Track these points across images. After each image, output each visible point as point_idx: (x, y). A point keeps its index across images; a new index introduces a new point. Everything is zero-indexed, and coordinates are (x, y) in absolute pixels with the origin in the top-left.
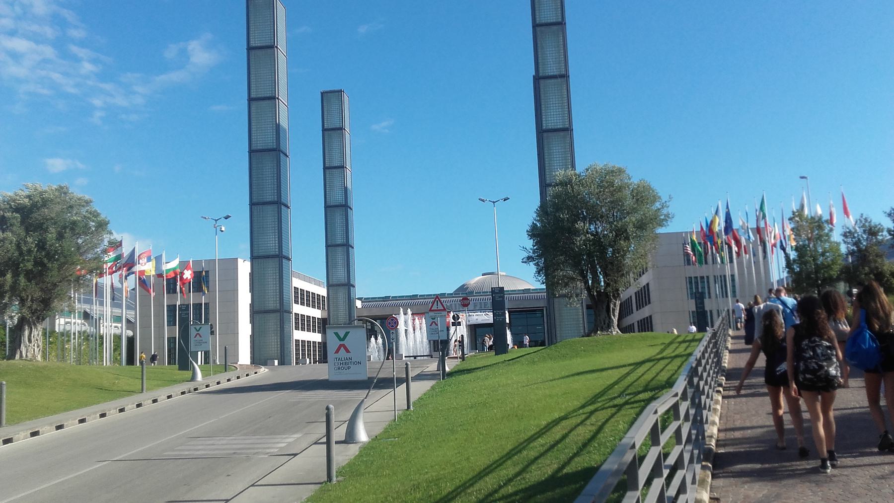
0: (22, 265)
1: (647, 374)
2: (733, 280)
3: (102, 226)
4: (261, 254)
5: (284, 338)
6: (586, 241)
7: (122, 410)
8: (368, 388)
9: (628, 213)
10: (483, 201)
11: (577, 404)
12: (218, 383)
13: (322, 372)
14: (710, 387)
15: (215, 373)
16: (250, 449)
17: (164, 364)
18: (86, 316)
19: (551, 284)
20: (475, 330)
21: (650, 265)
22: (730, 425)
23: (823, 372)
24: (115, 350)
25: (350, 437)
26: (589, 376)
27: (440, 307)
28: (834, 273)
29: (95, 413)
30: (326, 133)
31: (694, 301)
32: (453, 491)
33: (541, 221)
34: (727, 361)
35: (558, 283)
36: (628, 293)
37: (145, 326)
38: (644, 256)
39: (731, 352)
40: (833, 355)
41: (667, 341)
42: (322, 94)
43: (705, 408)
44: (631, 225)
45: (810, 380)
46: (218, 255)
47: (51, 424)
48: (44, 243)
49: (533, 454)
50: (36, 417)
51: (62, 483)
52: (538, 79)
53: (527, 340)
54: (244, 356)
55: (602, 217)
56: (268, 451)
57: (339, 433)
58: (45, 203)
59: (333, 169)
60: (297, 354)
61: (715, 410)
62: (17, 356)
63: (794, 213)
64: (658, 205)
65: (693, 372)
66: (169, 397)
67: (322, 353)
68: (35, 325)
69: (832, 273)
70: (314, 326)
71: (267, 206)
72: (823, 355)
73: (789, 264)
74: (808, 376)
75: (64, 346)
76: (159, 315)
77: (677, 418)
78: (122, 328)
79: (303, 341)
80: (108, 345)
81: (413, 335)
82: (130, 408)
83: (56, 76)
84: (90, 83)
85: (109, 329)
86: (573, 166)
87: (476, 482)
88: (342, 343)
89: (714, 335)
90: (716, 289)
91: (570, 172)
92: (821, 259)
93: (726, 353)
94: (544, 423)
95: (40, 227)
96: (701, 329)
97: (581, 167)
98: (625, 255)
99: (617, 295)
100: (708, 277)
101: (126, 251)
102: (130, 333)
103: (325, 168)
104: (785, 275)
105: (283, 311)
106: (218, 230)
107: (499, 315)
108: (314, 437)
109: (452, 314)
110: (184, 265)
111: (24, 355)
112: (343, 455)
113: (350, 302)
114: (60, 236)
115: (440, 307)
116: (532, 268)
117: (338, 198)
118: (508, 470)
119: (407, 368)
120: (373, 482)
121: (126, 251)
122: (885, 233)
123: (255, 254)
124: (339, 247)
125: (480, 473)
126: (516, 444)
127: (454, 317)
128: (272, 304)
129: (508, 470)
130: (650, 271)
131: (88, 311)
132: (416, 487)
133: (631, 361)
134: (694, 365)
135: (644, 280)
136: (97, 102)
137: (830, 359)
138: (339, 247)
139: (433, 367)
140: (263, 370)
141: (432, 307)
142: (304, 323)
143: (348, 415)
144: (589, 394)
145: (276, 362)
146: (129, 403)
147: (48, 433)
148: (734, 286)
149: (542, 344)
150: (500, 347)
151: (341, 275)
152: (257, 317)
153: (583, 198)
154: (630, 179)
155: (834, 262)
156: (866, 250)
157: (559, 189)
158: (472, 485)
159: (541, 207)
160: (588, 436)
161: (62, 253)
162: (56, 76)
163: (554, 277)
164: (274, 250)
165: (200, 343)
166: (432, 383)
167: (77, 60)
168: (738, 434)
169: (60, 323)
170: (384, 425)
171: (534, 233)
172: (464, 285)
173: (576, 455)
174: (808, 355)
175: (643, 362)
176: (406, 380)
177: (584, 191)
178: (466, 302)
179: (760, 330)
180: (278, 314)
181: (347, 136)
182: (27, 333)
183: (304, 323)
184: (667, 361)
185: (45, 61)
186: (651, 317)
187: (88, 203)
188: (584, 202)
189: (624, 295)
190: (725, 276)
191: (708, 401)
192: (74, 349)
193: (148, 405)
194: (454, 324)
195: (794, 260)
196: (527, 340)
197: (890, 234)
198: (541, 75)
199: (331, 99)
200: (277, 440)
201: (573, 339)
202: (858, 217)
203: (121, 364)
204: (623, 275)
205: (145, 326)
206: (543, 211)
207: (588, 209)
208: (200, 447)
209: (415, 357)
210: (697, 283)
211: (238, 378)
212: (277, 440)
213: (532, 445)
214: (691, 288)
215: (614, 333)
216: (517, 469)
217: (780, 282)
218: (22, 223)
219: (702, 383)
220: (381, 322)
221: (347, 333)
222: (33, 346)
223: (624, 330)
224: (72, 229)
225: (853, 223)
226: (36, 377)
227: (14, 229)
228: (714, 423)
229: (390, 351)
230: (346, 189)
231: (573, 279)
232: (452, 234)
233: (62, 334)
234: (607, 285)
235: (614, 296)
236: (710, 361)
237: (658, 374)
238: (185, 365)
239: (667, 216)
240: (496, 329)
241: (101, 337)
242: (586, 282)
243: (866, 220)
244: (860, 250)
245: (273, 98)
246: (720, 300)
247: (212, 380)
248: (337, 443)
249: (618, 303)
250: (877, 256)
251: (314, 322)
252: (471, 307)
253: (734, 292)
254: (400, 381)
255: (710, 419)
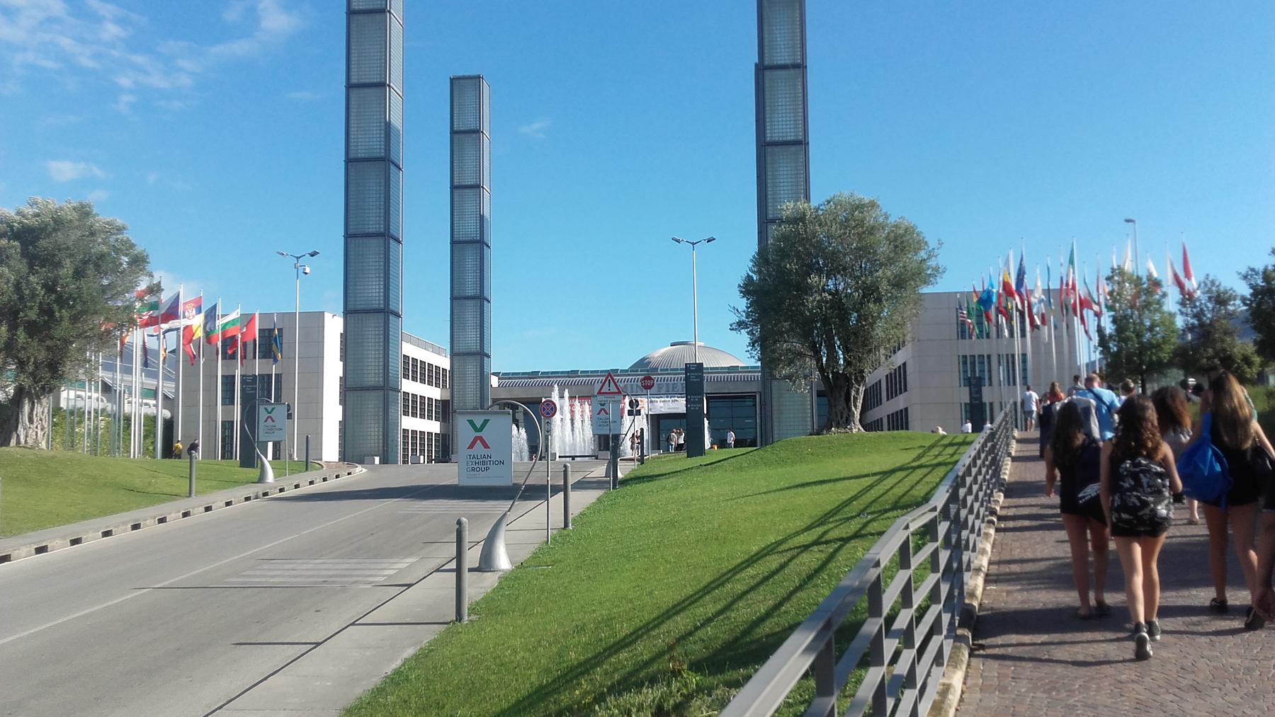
0: (21, 314)
1: (897, 487)
2: (1024, 361)
3: (139, 262)
4: (359, 307)
5: (388, 426)
6: (821, 302)
7: (162, 521)
8: (512, 498)
9: (881, 265)
10: (678, 241)
11: (800, 524)
12: (297, 486)
13: (447, 474)
14: (977, 517)
15: (292, 472)
16: (345, 576)
17: (215, 458)
18: (107, 389)
19: (769, 362)
20: (657, 420)
21: (908, 337)
22: (1006, 557)
23: (1147, 511)
24: (146, 437)
25: (486, 563)
26: (818, 488)
27: (614, 389)
28: (1165, 356)
29: (125, 523)
30: (456, 136)
31: (967, 389)
32: (632, 634)
33: (759, 272)
34: (1008, 471)
35: (779, 360)
36: (876, 375)
37: (191, 404)
38: (899, 326)
39: (1014, 459)
40: (1164, 486)
41: (927, 444)
42: (452, 80)
43: (967, 548)
44: (885, 282)
45: (1126, 521)
46: (299, 306)
47: (64, 538)
48: (55, 283)
49: (740, 588)
50: (42, 527)
51: (91, 614)
52: (762, 69)
53: (731, 437)
54: (330, 449)
55: (845, 269)
56: (371, 579)
57: (472, 556)
58: (59, 223)
59: (464, 189)
60: (405, 450)
61: (987, 535)
62: (13, 442)
63: (1113, 270)
64: (923, 254)
65: (959, 483)
66: (228, 504)
67: (444, 449)
68: (38, 398)
69: (1162, 355)
70: (430, 411)
71: (369, 239)
72: (1149, 486)
73: (1103, 341)
74: (1124, 516)
75: (73, 429)
76: (211, 389)
77: (935, 539)
78: (156, 406)
79: (414, 432)
80: (137, 430)
81: (571, 429)
82: (174, 518)
83: (66, 42)
84: (115, 53)
85: (136, 407)
86: (807, 198)
87: (663, 622)
88: (478, 434)
89: (992, 436)
90: (1000, 373)
91: (801, 205)
92: (1148, 335)
93: (1008, 461)
94: (755, 549)
95: (50, 261)
96: (977, 428)
97: (820, 194)
98: (874, 322)
99: (860, 378)
100: (989, 357)
101: (165, 297)
102: (168, 414)
103: (453, 188)
104: (1096, 356)
105: (387, 388)
106: (300, 271)
107: (695, 402)
108: (435, 563)
109: (627, 400)
110: (248, 320)
111: (22, 440)
112: (478, 587)
113: (483, 379)
114: (78, 274)
115: (614, 389)
116: (744, 337)
117: (469, 230)
118: (708, 607)
119: (565, 472)
120: (519, 622)
121: (165, 297)
122: (1238, 302)
123: (351, 307)
124: (469, 300)
125: (668, 611)
126: (717, 576)
127: (631, 404)
128: (373, 378)
129: (708, 607)
130: (909, 346)
131: (109, 382)
132: (581, 629)
133: (877, 469)
134: (960, 474)
135: (899, 359)
136: (125, 81)
137: (1159, 492)
138: (469, 300)
139: (599, 471)
140: (360, 470)
141: (602, 389)
142: (417, 406)
143: (485, 533)
144: (819, 512)
145: (377, 460)
146: (172, 511)
147: (60, 550)
148: (1025, 370)
149: (753, 444)
150: (693, 447)
151: (470, 340)
152: (350, 395)
153: (820, 242)
154: (887, 218)
155: (1165, 340)
156: (1210, 325)
157: (784, 228)
158: (657, 626)
159: (758, 254)
160: (815, 565)
161: (80, 297)
162: (66, 42)
163: (773, 351)
164: (377, 303)
165: (271, 430)
166: (597, 493)
167: (97, 19)
168: (1015, 568)
169: (67, 397)
170: (532, 549)
171: (748, 289)
172: (643, 359)
173: (799, 588)
174: (1127, 485)
175: (893, 471)
176: (564, 489)
177: (821, 234)
178: (649, 383)
179: (1060, 429)
180: (381, 393)
181: (486, 141)
182: (27, 408)
183: (417, 406)
184: (925, 471)
185: (52, 20)
186: (906, 409)
187: (120, 230)
188: (819, 247)
189: (870, 379)
190: (1013, 356)
191: (972, 537)
192: (89, 434)
193: (198, 514)
194: (630, 413)
195: (1111, 336)
196: (731, 437)
197: (1245, 304)
198: (766, 63)
199: (464, 87)
200: (379, 566)
201: (798, 438)
202: (1202, 279)
203: (154, 457)
204: (870, 351)
205: (191, 404)
206: (762, 259)
207: (825, 259)
208: (278, 573)
209: (573, 458)
210: (973, 364)
211: (325, 480)
212: (379, 566)
213: (738, 577)
214: (965, 371)
215: (855, 431)
216: (719, 607)
217: (1091, 365)
218: (25, 254)
219: (963, 513)
220: (531, 409)
221: (486, 422)
222: (34, 429)
223: (868, 427)
224: (97, 266)
225: (1196, 286)
226: (41, 471)
227: (12, 263)
228: (983, 552)
229: (536, 448)
230: (482, 217)
231: (801, 355)
232: (629, 286)
233: (72, 413)
234: (848, 363)
235: (856, 379)
236: (980, 478)
237: (912, 487)
238: (249, 459)
239: (936, 269)
240: (689, 422)
241: (128, 419)
242: (819, 360)
243: (1213, 283)
244: (1202, 325)
245: (382, 85)
246: (1004, 388)
247: (288, 482)
248: (470, 570)
249: (862, 389)
250: (1226, 333)
251: (430, 405)
252: (654, 390)
253: (1025, 378)
254: (556, 490)
255: (979, 546)
